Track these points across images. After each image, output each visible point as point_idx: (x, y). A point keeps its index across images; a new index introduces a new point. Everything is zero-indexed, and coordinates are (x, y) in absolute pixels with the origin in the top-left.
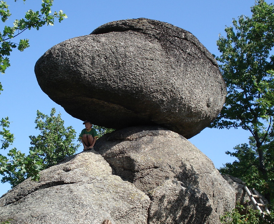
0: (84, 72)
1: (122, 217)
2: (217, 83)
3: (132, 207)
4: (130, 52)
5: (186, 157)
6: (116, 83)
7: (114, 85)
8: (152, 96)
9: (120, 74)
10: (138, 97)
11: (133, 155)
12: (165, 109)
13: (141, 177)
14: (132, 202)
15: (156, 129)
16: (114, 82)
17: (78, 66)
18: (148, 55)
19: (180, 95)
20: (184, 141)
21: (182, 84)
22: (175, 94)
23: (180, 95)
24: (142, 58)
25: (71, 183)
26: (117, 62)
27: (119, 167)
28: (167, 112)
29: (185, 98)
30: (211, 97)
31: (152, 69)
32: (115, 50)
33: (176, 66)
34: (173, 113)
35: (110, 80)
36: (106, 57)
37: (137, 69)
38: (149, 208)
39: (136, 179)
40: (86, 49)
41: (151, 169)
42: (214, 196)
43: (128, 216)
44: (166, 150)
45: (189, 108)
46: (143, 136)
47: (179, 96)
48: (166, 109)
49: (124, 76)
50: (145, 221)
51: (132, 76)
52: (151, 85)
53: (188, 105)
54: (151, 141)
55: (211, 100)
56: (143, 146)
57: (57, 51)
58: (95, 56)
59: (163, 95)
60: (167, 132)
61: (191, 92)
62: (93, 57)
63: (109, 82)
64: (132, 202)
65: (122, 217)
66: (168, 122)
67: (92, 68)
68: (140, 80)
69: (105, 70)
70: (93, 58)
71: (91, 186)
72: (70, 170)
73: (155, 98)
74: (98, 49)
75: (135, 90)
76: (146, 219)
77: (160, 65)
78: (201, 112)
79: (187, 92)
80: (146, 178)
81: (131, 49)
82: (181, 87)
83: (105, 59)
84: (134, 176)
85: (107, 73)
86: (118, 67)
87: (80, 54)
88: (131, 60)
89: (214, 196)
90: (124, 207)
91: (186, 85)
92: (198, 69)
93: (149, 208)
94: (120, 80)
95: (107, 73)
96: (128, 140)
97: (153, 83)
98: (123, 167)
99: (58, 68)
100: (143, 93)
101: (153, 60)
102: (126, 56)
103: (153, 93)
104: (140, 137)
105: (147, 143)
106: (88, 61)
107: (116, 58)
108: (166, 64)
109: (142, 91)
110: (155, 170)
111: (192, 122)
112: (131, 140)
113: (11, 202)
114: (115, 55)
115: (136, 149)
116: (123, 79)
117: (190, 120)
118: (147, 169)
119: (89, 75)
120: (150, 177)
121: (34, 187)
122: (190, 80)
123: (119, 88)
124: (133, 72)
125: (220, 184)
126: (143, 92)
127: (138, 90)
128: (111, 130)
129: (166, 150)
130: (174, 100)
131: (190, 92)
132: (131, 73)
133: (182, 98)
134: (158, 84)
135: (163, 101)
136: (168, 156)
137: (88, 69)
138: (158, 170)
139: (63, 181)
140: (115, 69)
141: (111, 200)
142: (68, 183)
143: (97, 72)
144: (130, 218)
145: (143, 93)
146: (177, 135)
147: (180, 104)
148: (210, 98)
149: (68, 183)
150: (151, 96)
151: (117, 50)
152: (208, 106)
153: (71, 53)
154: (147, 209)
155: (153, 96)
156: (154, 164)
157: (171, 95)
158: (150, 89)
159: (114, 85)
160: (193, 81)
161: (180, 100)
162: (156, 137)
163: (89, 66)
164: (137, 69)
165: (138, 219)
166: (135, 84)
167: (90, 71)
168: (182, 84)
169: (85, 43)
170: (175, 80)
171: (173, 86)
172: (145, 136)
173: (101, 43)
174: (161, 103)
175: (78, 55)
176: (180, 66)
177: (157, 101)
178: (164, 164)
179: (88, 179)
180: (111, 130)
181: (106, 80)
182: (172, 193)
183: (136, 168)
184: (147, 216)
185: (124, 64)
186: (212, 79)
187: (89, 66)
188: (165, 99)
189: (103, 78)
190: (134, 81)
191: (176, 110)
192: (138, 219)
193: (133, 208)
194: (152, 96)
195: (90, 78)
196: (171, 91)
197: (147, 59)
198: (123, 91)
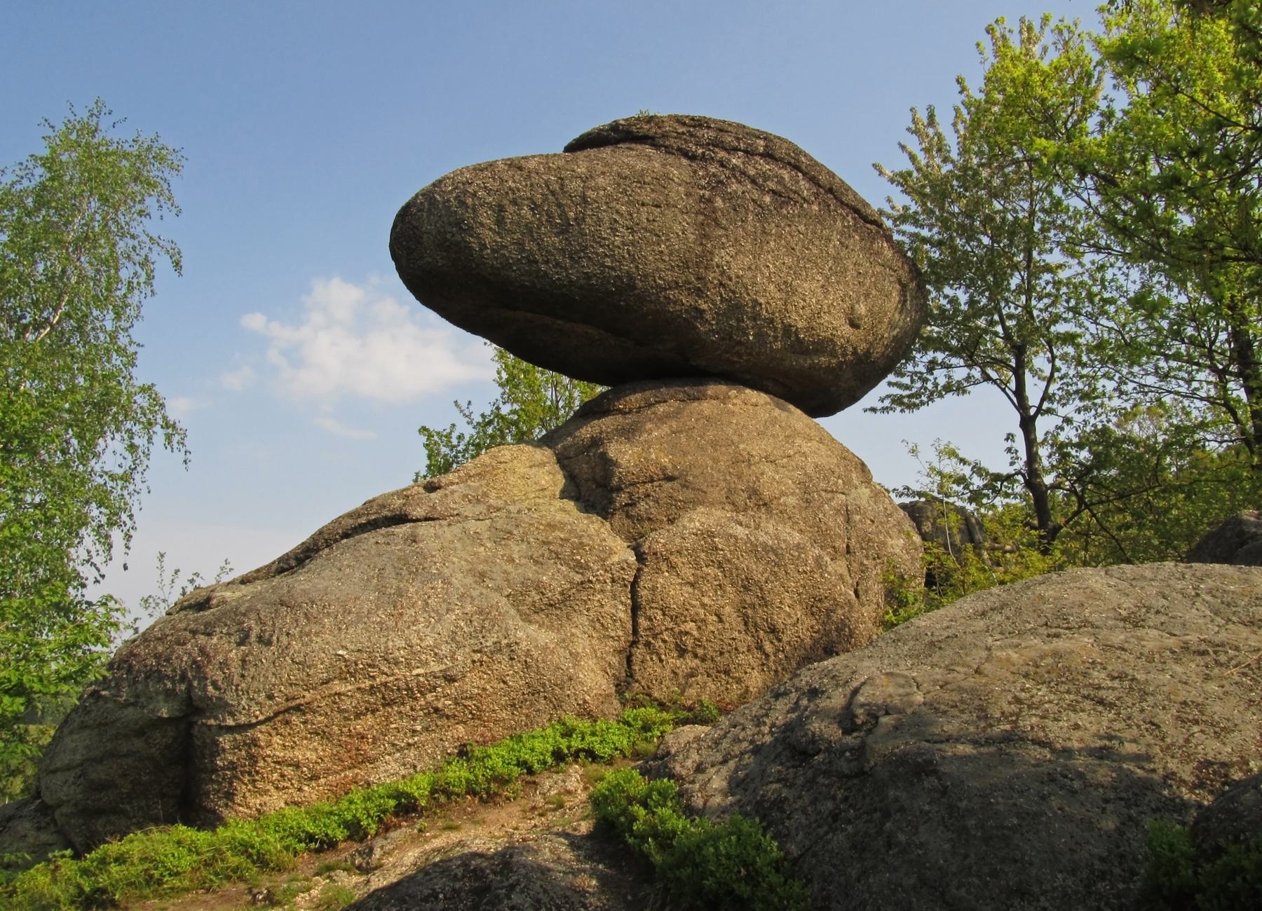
0: (480, 243)
1: (551, 605)
2: (878, 269)
3: (578, 578)
4: (596, 189)
5: (766, 452)
6: (561, 267)
7: (557, 273)
8: (665, 297)
9: (570, 243)
10: (624, 300)
13: (627, 505)
14: (581, 567)
16: (557, 264)
17: (465, 230)
18: (646, 196)
19: (748, 294)
20: (777, 412)
21: (753, 267)
22: (734, 292)
23: (748, 294)
24: (630, 203)
25: (427, 519)
26: (563, 215)
27: (587, 480)
28: (723, 339)
29: (768, 303)
30: (858, 302)
31: (657, 229)
32: (557, 187)
34: (740, 343)
35: (547, 262)
36: (534, 203)
37: (614, 230)
39: (615, 510)
40: (486, 187)
41: (655, 484)
42: (848, 552)
43: (567, 603)
44: (710, 435)
45: (787, 329)
46: (660, 402)
47: (747, 298)
48: (717, 333)
49: (583, 251)
50: (622, 615)
51: (601, 250)
52: (658, 270)
53: (783, 323)
54: (677, 414)
55: (862, 309)
58: (505, 202)
59: (698, 296)
60: (733, 392)
61: (788, 289)
62: (500, 206)
63: (543, 267)
64: (581, 567)
65: (551, 605)
66: (737, 366)
67: (499, 233)
68: (623, 257)
69: (533, 236)
70: (501, 208)
71: (482, 527)
72: (439, 487)
73: (675, 303)
74: (513, 185)
75: (614, 285)
76: (626, 611)
77: (680, 218)
78: (832, 340)
79: (772, 287)
80: (642, 506)
82: (749, 274)
83: (532, 209)
84: (611, 501)
85: (538, 244)
86: (564, 230)
87: (469, 201)
88: (598, 207)
89: (848, 552)
90: (555, 578)
92: (802, 228)
93: (634, 584)
94: (571, 258)
95: (538, 244)
96: (621, 412)
98: (594, 480)
99: (422, 238)
100: (636, 292)
101: (660, 207)
102: (584, 198)
103: (665, 289)
104: (650, 405)
106: (487, 218)
107: (559, 205)
108: (701, 218)
109: (634, 287)
111: (811, 367)
113: (286, 566)
114: (557, 199)
115: (628, 433)
116: (580, 258)
118: (645, 483)
119: (493, 251)
120: (651, 503)
121: (340, 531)
122: (776, 258)
123: (571, 281)
124: (605, 239)
125: (872, 521)
126: (636, 288)
127: (623, 282)
128: (600, 389)
129: (710, 435)
130: (734, 308)
131: (783, 287)
132: (600, 241)
133: (756, 303)
134: (678, 266)
137: (488, 236)
138: (676, 484)
139: (406, 515)
140: (557, 235)
141: (523, 561)
142: (418, 520)
143: (514, 244)
144: (577, 608)
145: (636, 292)
146: (761, 398)
148: (857, 306)
149: (418, 520)
150: (662, 299)
152: (854, 325)
153: (448, 201)
154: (625, 586)
156: (664, 469)
157: (721, 296)
158: (655, 281)
159: (557, 273)
161: (754, 307)
163: (490, 229)
164: (614, 230)
165: (600, 610)
166: (612, 268)
167: (495, 241)
168: (753, 267)
170: (728, 258)
171: (723, 273)
172: (665, 402)
173: (525, 173)
174: (695, 318)
176: (743, 221)
177: (681, 311)
178: (694, 469)
179: (481, 508)
180: (600, 389)
181: (536, 262)
182: (703, 542)
183: (615, 481)
184: (629, 601)
185: (580, 220)
187: (490, 229)
188: (704, 306)
189: (528, 256)
190: (608, 262)
192: (600, 610)
193: (582, 583)
194: (665, 297)
195: (496, 259)
196: (721, 284)
197: (643, 205)
198: (581, 288)
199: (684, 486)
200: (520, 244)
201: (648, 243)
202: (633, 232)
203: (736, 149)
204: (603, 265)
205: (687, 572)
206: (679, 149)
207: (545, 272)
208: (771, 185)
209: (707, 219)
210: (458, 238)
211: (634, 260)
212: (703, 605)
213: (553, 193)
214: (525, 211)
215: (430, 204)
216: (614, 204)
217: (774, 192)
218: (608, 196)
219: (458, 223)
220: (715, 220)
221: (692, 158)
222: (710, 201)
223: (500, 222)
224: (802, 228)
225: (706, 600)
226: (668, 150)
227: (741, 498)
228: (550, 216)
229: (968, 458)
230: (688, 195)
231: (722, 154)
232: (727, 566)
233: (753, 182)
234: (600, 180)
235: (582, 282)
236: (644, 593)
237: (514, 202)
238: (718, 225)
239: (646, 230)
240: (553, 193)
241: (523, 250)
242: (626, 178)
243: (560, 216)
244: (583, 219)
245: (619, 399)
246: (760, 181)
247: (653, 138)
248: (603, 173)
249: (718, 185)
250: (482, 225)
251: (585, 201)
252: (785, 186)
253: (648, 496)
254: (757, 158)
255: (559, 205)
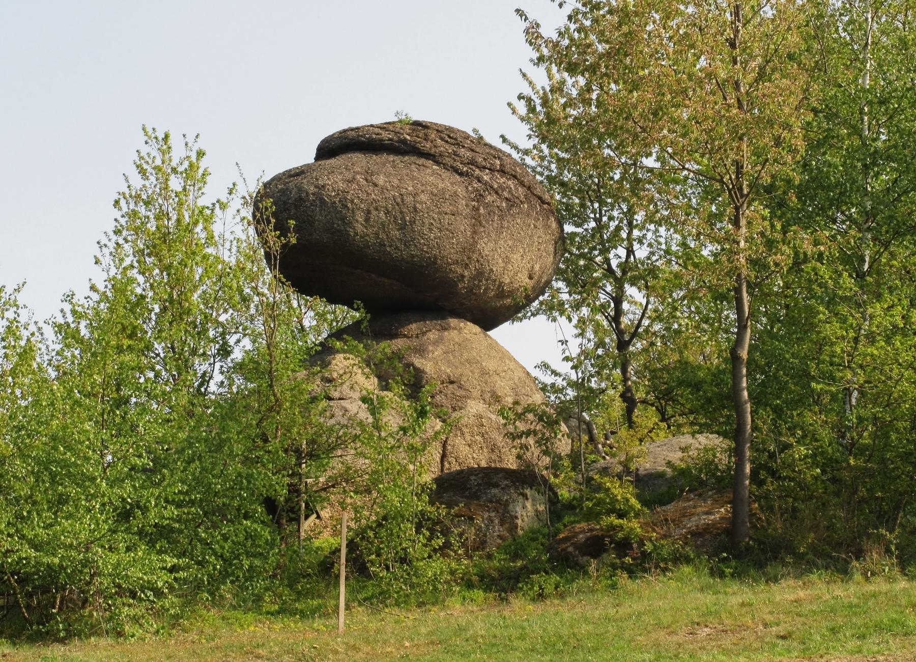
4: (421, 203)
11: (418, 362)
12: (464, 288)
15: (444, 318)
16: (397, 248)
18: (447, 208)
24: (439, 213)
26: (403, 218)
32: (399, 200)
33: (487, 221)
35: (391, 246)
37: (431, 230)
38: (446, 442)
44: (465, 356)
45: (501, 285)
52: (450, 253)
56: (430, 348)
57: (311, 197)
58: (372, 208)
60: (462, 325)
61: (507, 260)
63: (388, 249)
70: (369, 212)
79: (500, 261)
81: (423, 197)
82: (492, 253)
86: (402, 227)
87: (349, 205)
91: (499, 251)
92: (519, 221)
93: (446, 442)
94: (405, 245)
96: (405, 336)
97: (452, 251)
102: (415, 208)
105: (436, 343)
106: (360, 217)
107: (401, 212)
109: (435, 263)
110: (451, 386)
112: (408, 337)
115: (421, 351)
117: (499, 304)
119: (361, 237)
122: (506, 241)
129: (465, 356)
130: (480, 274)
133: (492, 270)
135: (463, 276)
136: (468, 366)
137: (359, 228)
138: (455, 386)
140: (398, 230)
147: (487, 280)
151: (403, 200)
152: (531, 278)
153: (335, 203)
155: (451, 270)
156: (449, 377)
160: (510, 243)
162: (446, 333)
164: (431, 230)
169: (354, 186)
175: (346, 206)
181: (385, 245)
185: (413, 222)
186: (541, 232)
191: (480, 289)
198: (407, 263)
199: (459, 387)
200: (377, 234)
201: (447, 238)
202: (441, 231)
203: (485, 168)
204: (422, 250)
205: (468, 437)
206: (452, 167)
207: (389, 253)
208: (506, 194)
209: (477, 221)
210: (342, 228)
211: (439, 248)
212: (473, 458)
213: (398, 204)
214: (382, 214)
215: (321, 202)
216: (431, 214)
217: (507, 199)
218: (428, 208)
219: (343, 219)
220: (480, 222)
221: (461, 174)
222: (478, 209)
223: (367, 220)
224: (519, 221)
225: (475, 455)
226: (445, 167)
227: (487, 396)
228: (395, 218)
229: (559, 371)
230: (467, 205)
231: (477, 172)
232: (486, 436)
233: (497, 193)
234: (422, 196)
235: (409, 259)
236: (449, 447)
237: (376, 209)
238: (481, 225)
239: (447, 230)
240: (398, 204)
241: (378, 238)
242: (436, 195)
243: (401, 219)
244: (414, 222)
245: (403, 327)
246: (500, 192)
247: (434, 156)
248: (423, 191)
249: (480, 197)
250: (357, 221)
251: (416, 211)
252: (512, 195)
253: (441, 392)
254: (496, 173)
255: (401, 212)
